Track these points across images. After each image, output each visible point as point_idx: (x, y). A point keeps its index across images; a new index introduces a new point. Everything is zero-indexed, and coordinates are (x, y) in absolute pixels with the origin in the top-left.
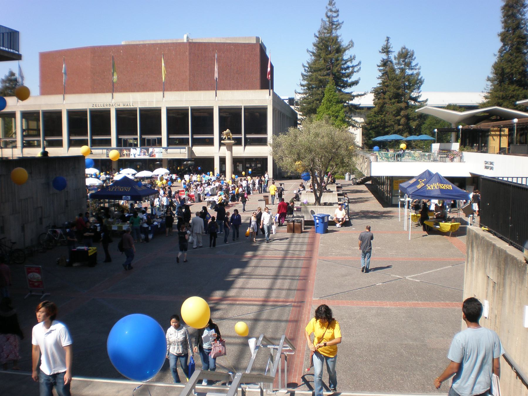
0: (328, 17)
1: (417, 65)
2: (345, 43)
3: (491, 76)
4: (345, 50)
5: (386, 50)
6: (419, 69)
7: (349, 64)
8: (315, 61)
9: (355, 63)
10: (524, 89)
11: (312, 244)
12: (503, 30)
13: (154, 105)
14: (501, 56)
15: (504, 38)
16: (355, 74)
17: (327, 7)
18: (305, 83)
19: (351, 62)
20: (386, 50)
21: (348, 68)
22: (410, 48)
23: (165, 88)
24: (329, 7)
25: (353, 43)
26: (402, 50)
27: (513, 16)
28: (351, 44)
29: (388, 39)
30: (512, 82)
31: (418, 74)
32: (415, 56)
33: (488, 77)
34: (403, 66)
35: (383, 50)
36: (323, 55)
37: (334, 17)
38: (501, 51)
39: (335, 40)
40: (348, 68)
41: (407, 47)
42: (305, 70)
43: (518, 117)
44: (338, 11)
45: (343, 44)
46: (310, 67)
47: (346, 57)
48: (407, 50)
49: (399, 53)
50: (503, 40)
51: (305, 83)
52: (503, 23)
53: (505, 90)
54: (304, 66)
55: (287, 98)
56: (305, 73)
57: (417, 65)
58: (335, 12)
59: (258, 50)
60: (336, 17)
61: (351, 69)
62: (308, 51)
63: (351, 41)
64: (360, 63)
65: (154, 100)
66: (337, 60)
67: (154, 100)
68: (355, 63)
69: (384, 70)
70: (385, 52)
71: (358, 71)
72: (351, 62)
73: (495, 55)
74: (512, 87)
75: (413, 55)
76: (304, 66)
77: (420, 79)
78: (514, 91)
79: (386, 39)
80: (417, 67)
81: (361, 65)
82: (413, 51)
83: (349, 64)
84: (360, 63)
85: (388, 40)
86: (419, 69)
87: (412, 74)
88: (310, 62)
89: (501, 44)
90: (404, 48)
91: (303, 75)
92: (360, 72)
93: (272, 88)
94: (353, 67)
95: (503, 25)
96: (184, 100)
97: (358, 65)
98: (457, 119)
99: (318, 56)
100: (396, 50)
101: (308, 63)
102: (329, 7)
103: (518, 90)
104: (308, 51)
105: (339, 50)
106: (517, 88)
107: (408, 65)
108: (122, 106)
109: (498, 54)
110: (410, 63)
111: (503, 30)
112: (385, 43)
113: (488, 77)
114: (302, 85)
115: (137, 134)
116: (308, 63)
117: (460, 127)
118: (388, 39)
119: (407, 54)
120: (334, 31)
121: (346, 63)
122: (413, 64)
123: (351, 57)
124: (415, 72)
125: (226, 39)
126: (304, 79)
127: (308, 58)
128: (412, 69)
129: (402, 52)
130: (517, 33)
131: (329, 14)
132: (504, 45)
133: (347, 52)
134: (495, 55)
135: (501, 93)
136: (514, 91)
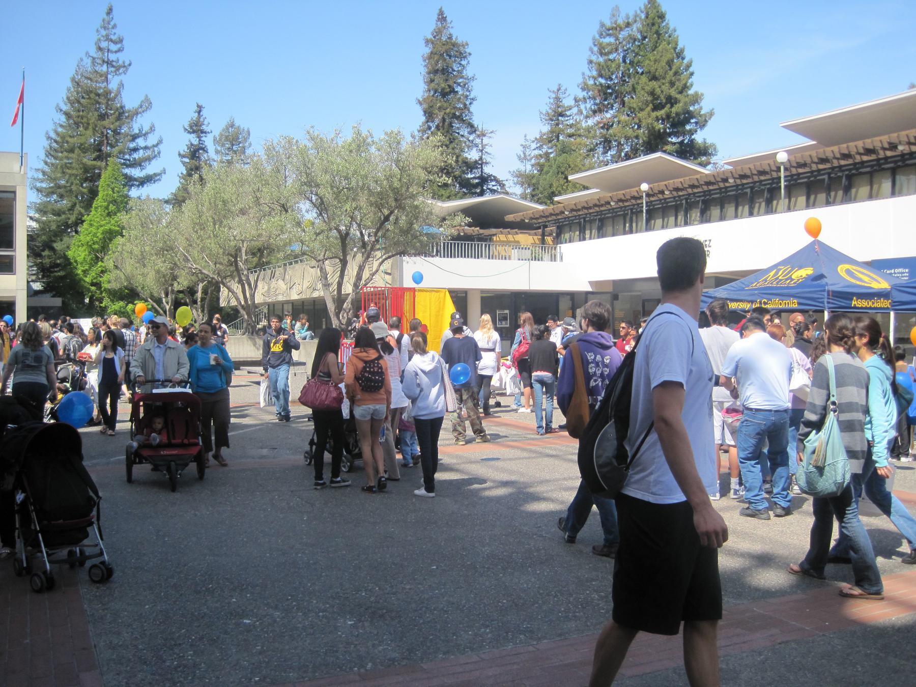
0: (100, 49)
2: (129, 101)
5: (196, 128)
7: (141, 142)
9: (152, 140)
11: (571, 461)
17: (98, 31)
19: (146, 139)
20: (196, 128)
24: (104, 33)
27: (445, 71)
28: (146, 105)
29: (200, 110)
37: (112, 52)
44: (121, 41)
58: (115, 43)
60: (116, 52)
64: (160, 142)
68: (152, 140)
70: (194, 132)
79: (196, 108)
84: (160, 142)
85: (199, 112)
89: (423, 119)
94: (146, 148)
102: (104, 33)
117: (645, 187)
118: (200, 110)
131: (104, 45)
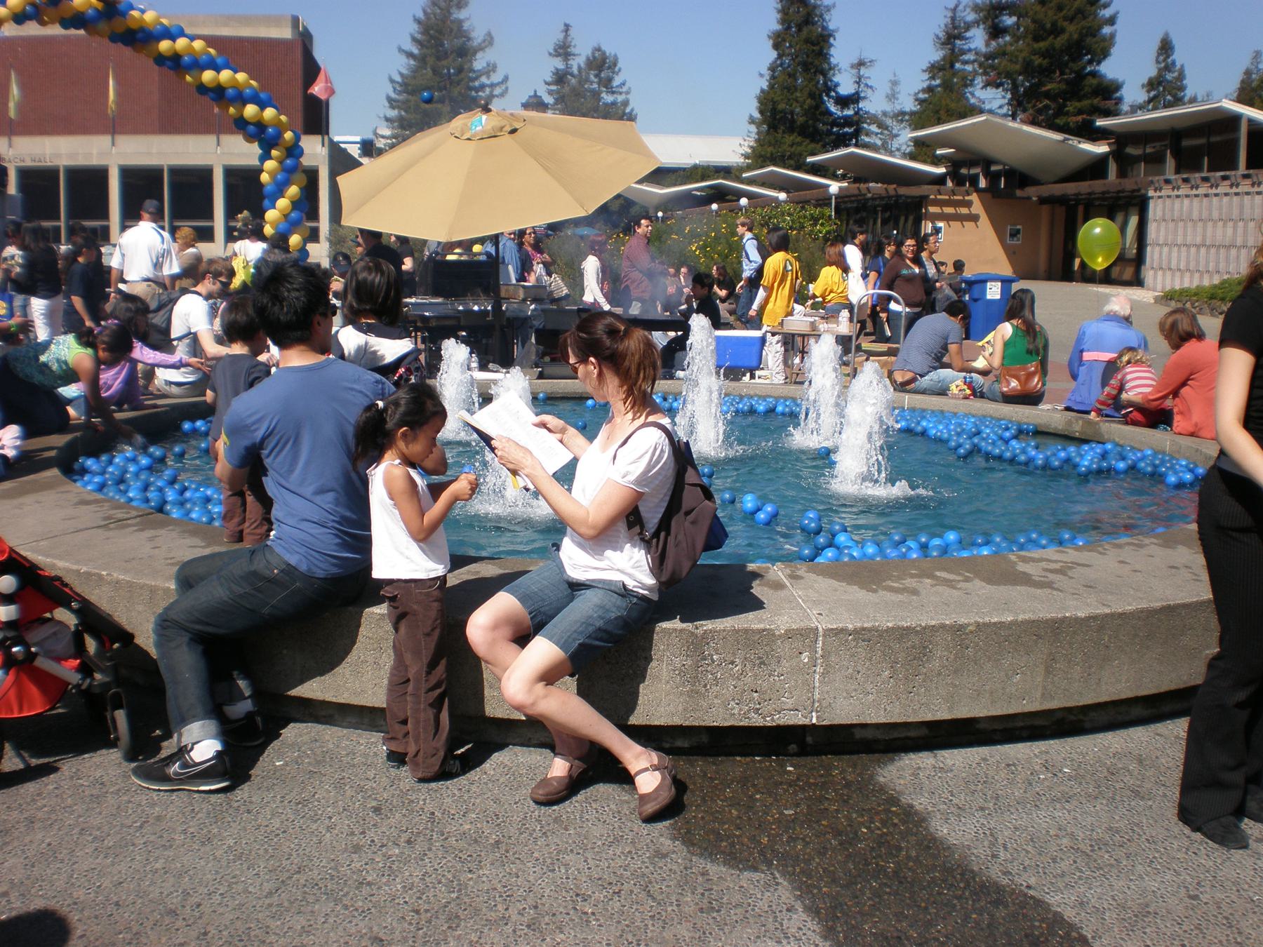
1: (623, 84)
2: (478, 36)
3: (757, 115)
4: (475, 53)
5: (563, 50)
6: (627, 93)
7: (484, 80)
8: (415, 71)
9: (496, 78)
10: (812, 141)
12: (778, 27)
13: (95, 161)
14: (773, 77)
15: (778, 42)
16: (495, 101)
18: (393, 113)
19: (488, 77)
20: (563, 50)
21: (482, 87)
22: (609, 49)
23: (114, 127)
25: (492, 38)
26: (593, 53)
28: (489, 40)
29: (567, 27)
30: (791, 129)
31: (626, 103)
32: (619, 65)
33: (751, 116)
34: (595, 86)
35: (555, 50)
36: (431, 61)
38: (772, 69)
39: (459, 30)
40: (482, 87)
41: (603, 48)
42: (395, 89)
43: (750, 196)
45: (473, 35)
46: (405, 85)
47: (479, 63)
48: (604, 53)
49: (588, 59)
50: (776, 46)
51: (393, 113)
52: (779, 12)
53: (776, 143)
54: (392, 81)
55: (358, 139)
56: (393, 95)
57: (623, 84)
59: (299, 54)
61: (488, 90)
62: (400, 50)
63: (489, 34)
64: (506, 79)
65: (95, 152)
66: (460, 70)
67: (95, 152)
68: (496, 78)
69: (558, 92)
71: (502, 95)
72: (488, 77)
73: (761, 75)
74: (789, 139)
75: (615, 65)
76: (392, 81)
77: (630, 113)
78: (792, 146)
79: (562, 27)
80: (624, 89)
81: (509, 84)
82: (615, 56)
83: (484, 80)
84: (506, 79)
86: (627, 93)
87: (614, 103)
88: (405, 71)
90: (599, 49)
91: (390, 100)
92: (507, 97)
93: (328, 133)
94: (492, 86)
95: (779, 16)
96: (154, 151)
97: (502, 83)
98: (655, 201)
99: (421, 60)
100: (582, 52)
101: (401, 75)
103: (800, 144)
104: (400, 50)
105: (465, 52)
106: (799, 139)
107: (607, 83)
108: (29, 163)
109: (767, 74)
110: (610, 80)
111: (778, 27)
112: (561, 36)
113: (751, 116)
114: (387, 119)
115: (58, 218)
116: (401, 75)
119: (604, 62)
120: (454, 10)
121: (477, 78)
122: (617, 82)
123: (488, 65)
124: (620, 98)
125: (229, 19)
126: (393, 107)
127: (399, 66)
128: (613, 93)
129: (594, 57)
130: (805, 30)
132: (780, 56)
133: (479, 55)
134: (761, 75)
135: (770, 149)
136: (792, 146)
